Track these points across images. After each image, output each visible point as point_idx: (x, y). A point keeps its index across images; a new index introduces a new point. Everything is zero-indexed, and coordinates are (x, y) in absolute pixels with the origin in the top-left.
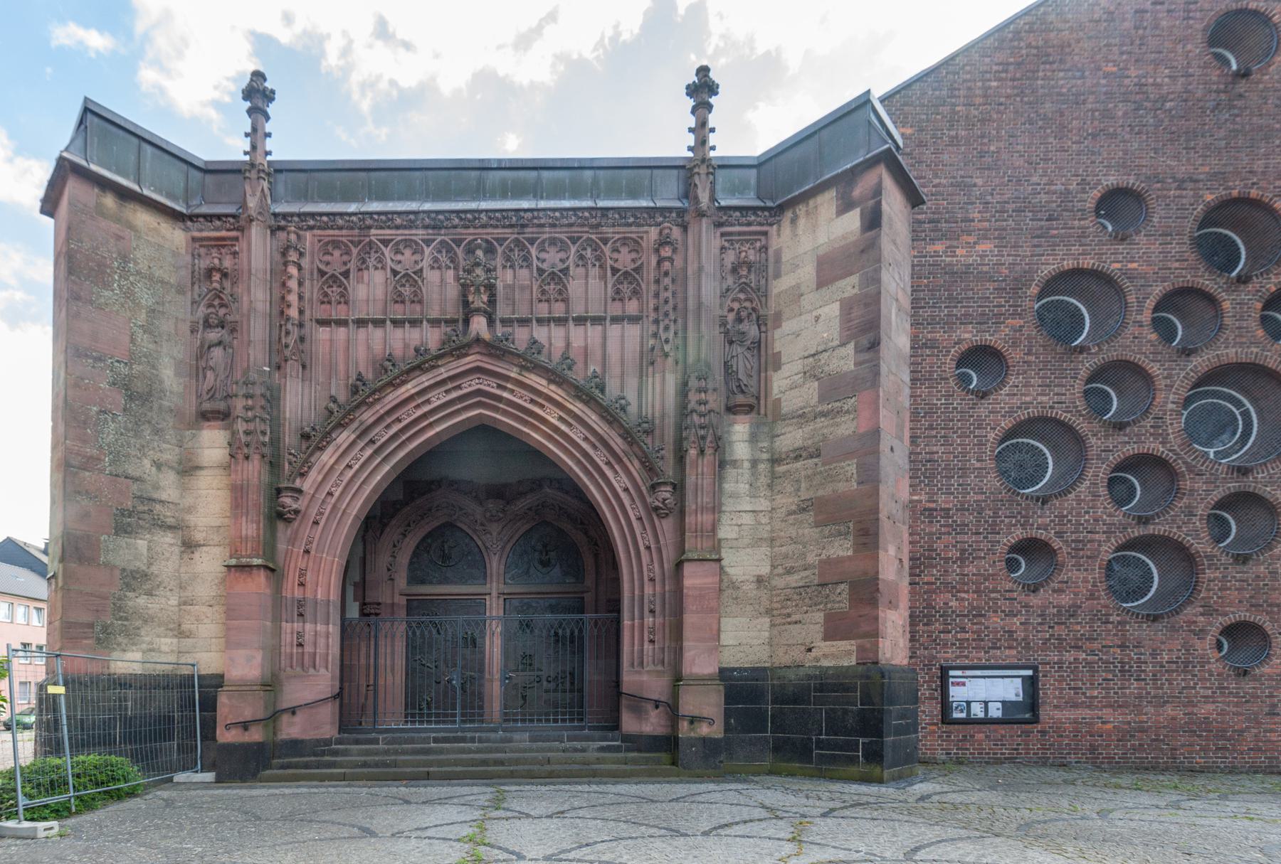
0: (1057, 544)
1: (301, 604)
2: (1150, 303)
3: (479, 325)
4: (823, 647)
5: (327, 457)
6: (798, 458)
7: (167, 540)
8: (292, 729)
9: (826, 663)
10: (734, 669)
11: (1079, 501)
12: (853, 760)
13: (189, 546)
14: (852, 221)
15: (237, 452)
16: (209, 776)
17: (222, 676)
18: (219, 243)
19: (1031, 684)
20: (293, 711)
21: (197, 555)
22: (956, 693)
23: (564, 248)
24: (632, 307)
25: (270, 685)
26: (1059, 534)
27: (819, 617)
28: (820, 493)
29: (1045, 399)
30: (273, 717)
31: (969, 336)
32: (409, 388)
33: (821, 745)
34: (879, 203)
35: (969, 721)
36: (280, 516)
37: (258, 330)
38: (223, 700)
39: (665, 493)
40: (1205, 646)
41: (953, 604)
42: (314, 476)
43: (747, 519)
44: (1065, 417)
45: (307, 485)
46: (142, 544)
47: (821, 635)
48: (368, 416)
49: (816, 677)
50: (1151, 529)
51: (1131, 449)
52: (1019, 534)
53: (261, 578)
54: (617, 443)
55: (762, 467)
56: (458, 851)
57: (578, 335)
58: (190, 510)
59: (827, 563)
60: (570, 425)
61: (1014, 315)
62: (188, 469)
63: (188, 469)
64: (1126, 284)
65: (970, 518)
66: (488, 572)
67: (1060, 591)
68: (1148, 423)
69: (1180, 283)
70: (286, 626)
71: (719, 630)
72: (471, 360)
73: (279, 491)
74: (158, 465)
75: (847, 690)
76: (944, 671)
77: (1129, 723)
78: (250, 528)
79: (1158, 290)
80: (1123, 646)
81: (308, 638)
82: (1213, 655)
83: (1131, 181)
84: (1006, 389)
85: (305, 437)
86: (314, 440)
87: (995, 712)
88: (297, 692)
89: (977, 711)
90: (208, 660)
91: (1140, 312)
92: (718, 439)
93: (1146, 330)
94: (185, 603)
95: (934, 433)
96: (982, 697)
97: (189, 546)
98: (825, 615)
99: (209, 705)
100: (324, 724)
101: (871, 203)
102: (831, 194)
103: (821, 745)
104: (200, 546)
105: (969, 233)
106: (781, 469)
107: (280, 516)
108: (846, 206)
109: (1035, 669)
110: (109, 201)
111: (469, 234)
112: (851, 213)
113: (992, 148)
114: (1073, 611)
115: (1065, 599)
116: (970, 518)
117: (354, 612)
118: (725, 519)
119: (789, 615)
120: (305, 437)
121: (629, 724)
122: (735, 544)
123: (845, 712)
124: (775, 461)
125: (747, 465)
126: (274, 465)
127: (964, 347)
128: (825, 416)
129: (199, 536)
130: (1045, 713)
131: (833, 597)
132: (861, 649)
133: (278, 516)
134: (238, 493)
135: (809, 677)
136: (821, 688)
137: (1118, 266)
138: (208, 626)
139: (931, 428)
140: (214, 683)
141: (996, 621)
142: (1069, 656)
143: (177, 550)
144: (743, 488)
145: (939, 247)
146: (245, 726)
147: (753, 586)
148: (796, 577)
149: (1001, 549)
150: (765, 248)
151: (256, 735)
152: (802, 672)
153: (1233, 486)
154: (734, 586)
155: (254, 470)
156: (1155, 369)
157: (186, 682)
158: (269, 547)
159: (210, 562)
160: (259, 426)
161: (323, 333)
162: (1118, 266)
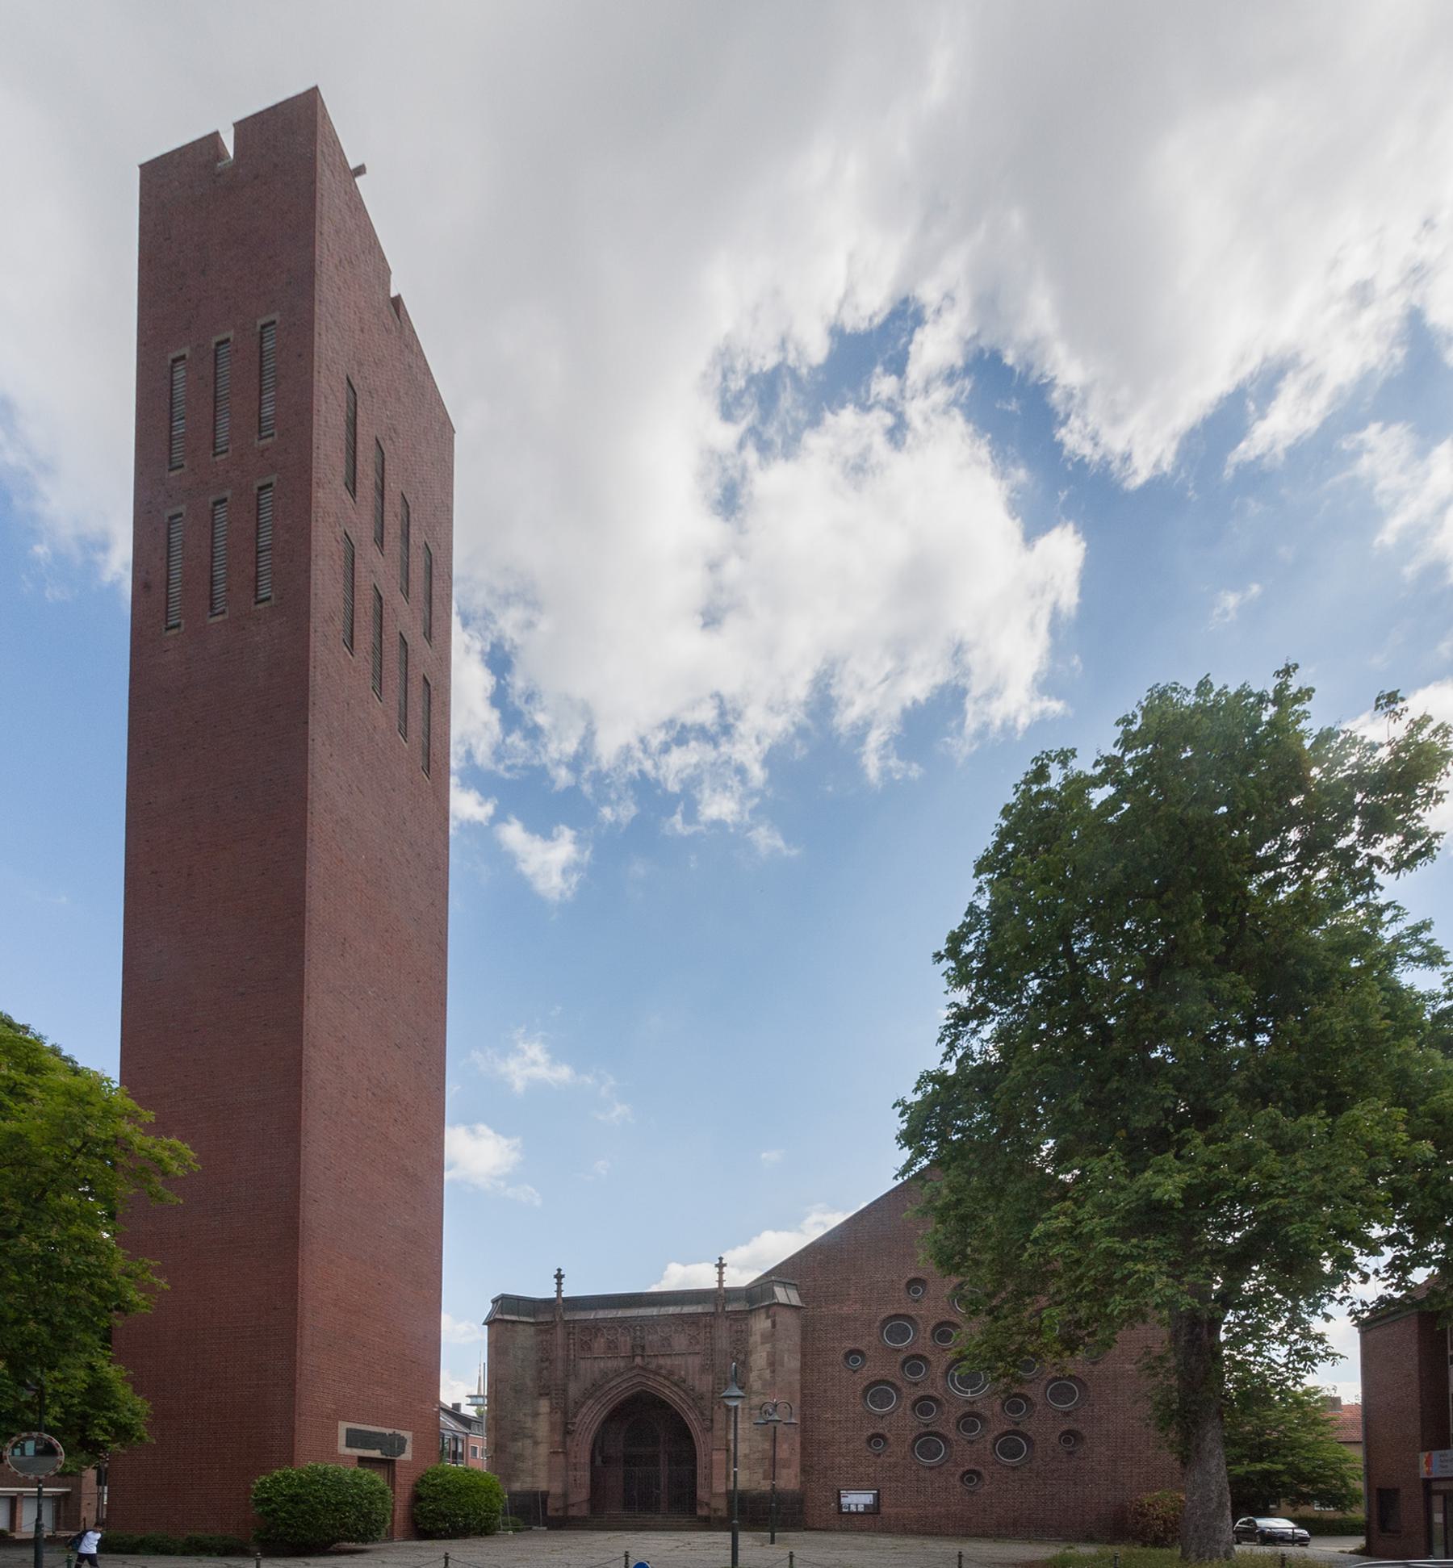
1: (575, 1464)
2: (929, 1329)
3: (638, 1360)
5: (584, 1410)
7: (528, 1442)
8: (573, 1512)
11: (898, 1416)
14: (768, 1323)
15: (552, 1410)
16: (545, 1528)
17: (548, 1492)
18: (546, 1331)
19: (877, 1498)
20: (573, 1505)
22: (844, 1501)
23: (670, 1327)
24: (697, 1348)
25: (565, 1495)
30: (566, 1507)
31: (850, 1345)
32: (613, 1383)
35: (850, 1513)
36: (568, 1433)
37: (560, 1365)
38: (549, 1500)
39: (708, 1422)
40: (955, 1481)
41: (843, 1462)
42: (579, 1417)
45: (577, 1420)
46: (520, 1444)
48: (598, 1394)
50: (930, 1429)
51: (921, 1393)
52: (871, 1431)
53: (561, 1456)
54: (690, 1402)
55: (747, 1410)
56: (66, 1567)
57: (678, 1361)
62: (536, 1415)
63: (536, 1415)
64: (919, 1321)
65: (850, 1425)
68: (929, 1381)
69: (943, 1319)
70: (570, 1473)
72: (635, 1372)
73: (567, 1423)
74: (525, 1414)
76: (839, 1491)
78: (558, 1438)
79: (933, 1323)
80: (918, 1480)
81: (578, 1477)
82: (958, 1484)
83: (920, 1275)
84: (866, 1368)
85: (576, 1403)
86: (579, 1405)
87: (861, 1509)
88: (573, 1499)
89: (853, 1508)
90: (543, 1486)
91: (925, 1333)
93: (927, 1340)
96: (855, 1502)
97: (536, 1443)
99: (545, 1502)
100: (583, 1511)
102: (763, 1311)
104: (658, 727)
105: (849, 1300)
106: (752, 1412)
107: (568, 1433)
108: (768, 1317)
109: (878, 1490)
110: (509, 1326)
112: (798, 1299)
114: (896, 1465)
115: (892, 1460)
116: (850, 1425)
117: (599, 1459)
120: (576, 1403)
121: (700, 1512)
124: (751, 1409)
126: (565, 1413)
127: (847, 1350)
129: (539, 1440)
130: (883, 1509)
133: (567, 1433)
134: (553, 1426)
138: (542, 1473)
139: (833, 1386)
140: (545, 1495)
141: (862, 1469)
142: (894, 1484)
145: (836, 1307)
146: (557, 1510)
149: (864, 1438)
150: (747, 1324)
151: (560, 1513)
153: (967, 1409)
155: (558, 1417)
156: (932, 1358)
157: (535, 1494)
158: (564, 1444)
159: (543, 1450)
160: (560, 1400)
161: (582, 1362)
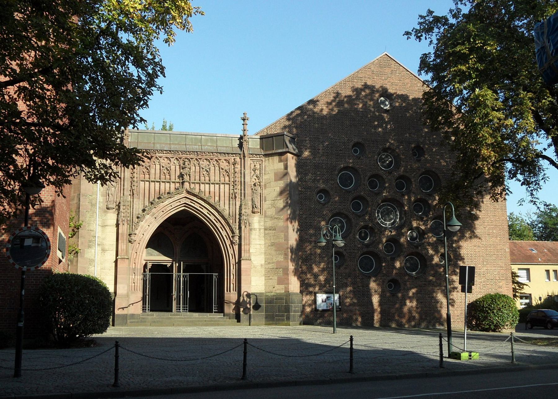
0: (345, 253)
4: (277, 287)
6: (270, 230)
9: (278, 292)
10: (227, 325)
12: (283, 320)
13: (104, 250)
21: (106, 254)
26: (345, 250)
27: (276, 278)
28: (276, 241)
29: (341, 207)
33: (277, 316)
34: (287, 163)
43: (258, 246)
44: (346, 213)
47: (276, 283)
49: (275, 296)
58: (104, 239)
59: (278, 262)
60: (210, 215)
61: (332, 180)
66: (175, 252)
67: (346, 268)
71: (251, 281)
75: (282, 300)
77: (365, 311)
79: (369, 174)
92: (249, 224)
94: (102, 269)
95: (311, 216)
97: (104, 250)
98: (278, 278)
101: (286, 162)
103: (277, 316)
111: (184, 156)
113: (325, 128)
118: (252, 246)
119: (269, 277)
122: (255, 254)
123: (282, 306)
125: (258, 230)
128: (276, 219)
129: (107, 247)
131: (279, 272)
132: (285, 288)
135: (274, 296)
136: (276, 299)
137: (358, 166)
139: (310, 215)
143: (100, 252)
144: (257, 237)
147: (260, 267)
148: (270, 265)
152: (272, 294)
154: (255, 267)
156: (369, 199)
162: (358, 166)
